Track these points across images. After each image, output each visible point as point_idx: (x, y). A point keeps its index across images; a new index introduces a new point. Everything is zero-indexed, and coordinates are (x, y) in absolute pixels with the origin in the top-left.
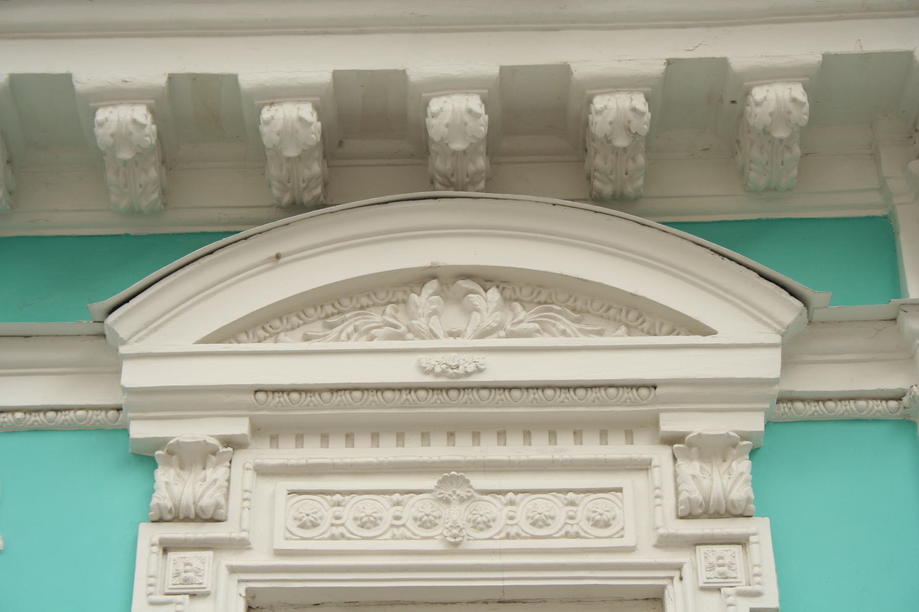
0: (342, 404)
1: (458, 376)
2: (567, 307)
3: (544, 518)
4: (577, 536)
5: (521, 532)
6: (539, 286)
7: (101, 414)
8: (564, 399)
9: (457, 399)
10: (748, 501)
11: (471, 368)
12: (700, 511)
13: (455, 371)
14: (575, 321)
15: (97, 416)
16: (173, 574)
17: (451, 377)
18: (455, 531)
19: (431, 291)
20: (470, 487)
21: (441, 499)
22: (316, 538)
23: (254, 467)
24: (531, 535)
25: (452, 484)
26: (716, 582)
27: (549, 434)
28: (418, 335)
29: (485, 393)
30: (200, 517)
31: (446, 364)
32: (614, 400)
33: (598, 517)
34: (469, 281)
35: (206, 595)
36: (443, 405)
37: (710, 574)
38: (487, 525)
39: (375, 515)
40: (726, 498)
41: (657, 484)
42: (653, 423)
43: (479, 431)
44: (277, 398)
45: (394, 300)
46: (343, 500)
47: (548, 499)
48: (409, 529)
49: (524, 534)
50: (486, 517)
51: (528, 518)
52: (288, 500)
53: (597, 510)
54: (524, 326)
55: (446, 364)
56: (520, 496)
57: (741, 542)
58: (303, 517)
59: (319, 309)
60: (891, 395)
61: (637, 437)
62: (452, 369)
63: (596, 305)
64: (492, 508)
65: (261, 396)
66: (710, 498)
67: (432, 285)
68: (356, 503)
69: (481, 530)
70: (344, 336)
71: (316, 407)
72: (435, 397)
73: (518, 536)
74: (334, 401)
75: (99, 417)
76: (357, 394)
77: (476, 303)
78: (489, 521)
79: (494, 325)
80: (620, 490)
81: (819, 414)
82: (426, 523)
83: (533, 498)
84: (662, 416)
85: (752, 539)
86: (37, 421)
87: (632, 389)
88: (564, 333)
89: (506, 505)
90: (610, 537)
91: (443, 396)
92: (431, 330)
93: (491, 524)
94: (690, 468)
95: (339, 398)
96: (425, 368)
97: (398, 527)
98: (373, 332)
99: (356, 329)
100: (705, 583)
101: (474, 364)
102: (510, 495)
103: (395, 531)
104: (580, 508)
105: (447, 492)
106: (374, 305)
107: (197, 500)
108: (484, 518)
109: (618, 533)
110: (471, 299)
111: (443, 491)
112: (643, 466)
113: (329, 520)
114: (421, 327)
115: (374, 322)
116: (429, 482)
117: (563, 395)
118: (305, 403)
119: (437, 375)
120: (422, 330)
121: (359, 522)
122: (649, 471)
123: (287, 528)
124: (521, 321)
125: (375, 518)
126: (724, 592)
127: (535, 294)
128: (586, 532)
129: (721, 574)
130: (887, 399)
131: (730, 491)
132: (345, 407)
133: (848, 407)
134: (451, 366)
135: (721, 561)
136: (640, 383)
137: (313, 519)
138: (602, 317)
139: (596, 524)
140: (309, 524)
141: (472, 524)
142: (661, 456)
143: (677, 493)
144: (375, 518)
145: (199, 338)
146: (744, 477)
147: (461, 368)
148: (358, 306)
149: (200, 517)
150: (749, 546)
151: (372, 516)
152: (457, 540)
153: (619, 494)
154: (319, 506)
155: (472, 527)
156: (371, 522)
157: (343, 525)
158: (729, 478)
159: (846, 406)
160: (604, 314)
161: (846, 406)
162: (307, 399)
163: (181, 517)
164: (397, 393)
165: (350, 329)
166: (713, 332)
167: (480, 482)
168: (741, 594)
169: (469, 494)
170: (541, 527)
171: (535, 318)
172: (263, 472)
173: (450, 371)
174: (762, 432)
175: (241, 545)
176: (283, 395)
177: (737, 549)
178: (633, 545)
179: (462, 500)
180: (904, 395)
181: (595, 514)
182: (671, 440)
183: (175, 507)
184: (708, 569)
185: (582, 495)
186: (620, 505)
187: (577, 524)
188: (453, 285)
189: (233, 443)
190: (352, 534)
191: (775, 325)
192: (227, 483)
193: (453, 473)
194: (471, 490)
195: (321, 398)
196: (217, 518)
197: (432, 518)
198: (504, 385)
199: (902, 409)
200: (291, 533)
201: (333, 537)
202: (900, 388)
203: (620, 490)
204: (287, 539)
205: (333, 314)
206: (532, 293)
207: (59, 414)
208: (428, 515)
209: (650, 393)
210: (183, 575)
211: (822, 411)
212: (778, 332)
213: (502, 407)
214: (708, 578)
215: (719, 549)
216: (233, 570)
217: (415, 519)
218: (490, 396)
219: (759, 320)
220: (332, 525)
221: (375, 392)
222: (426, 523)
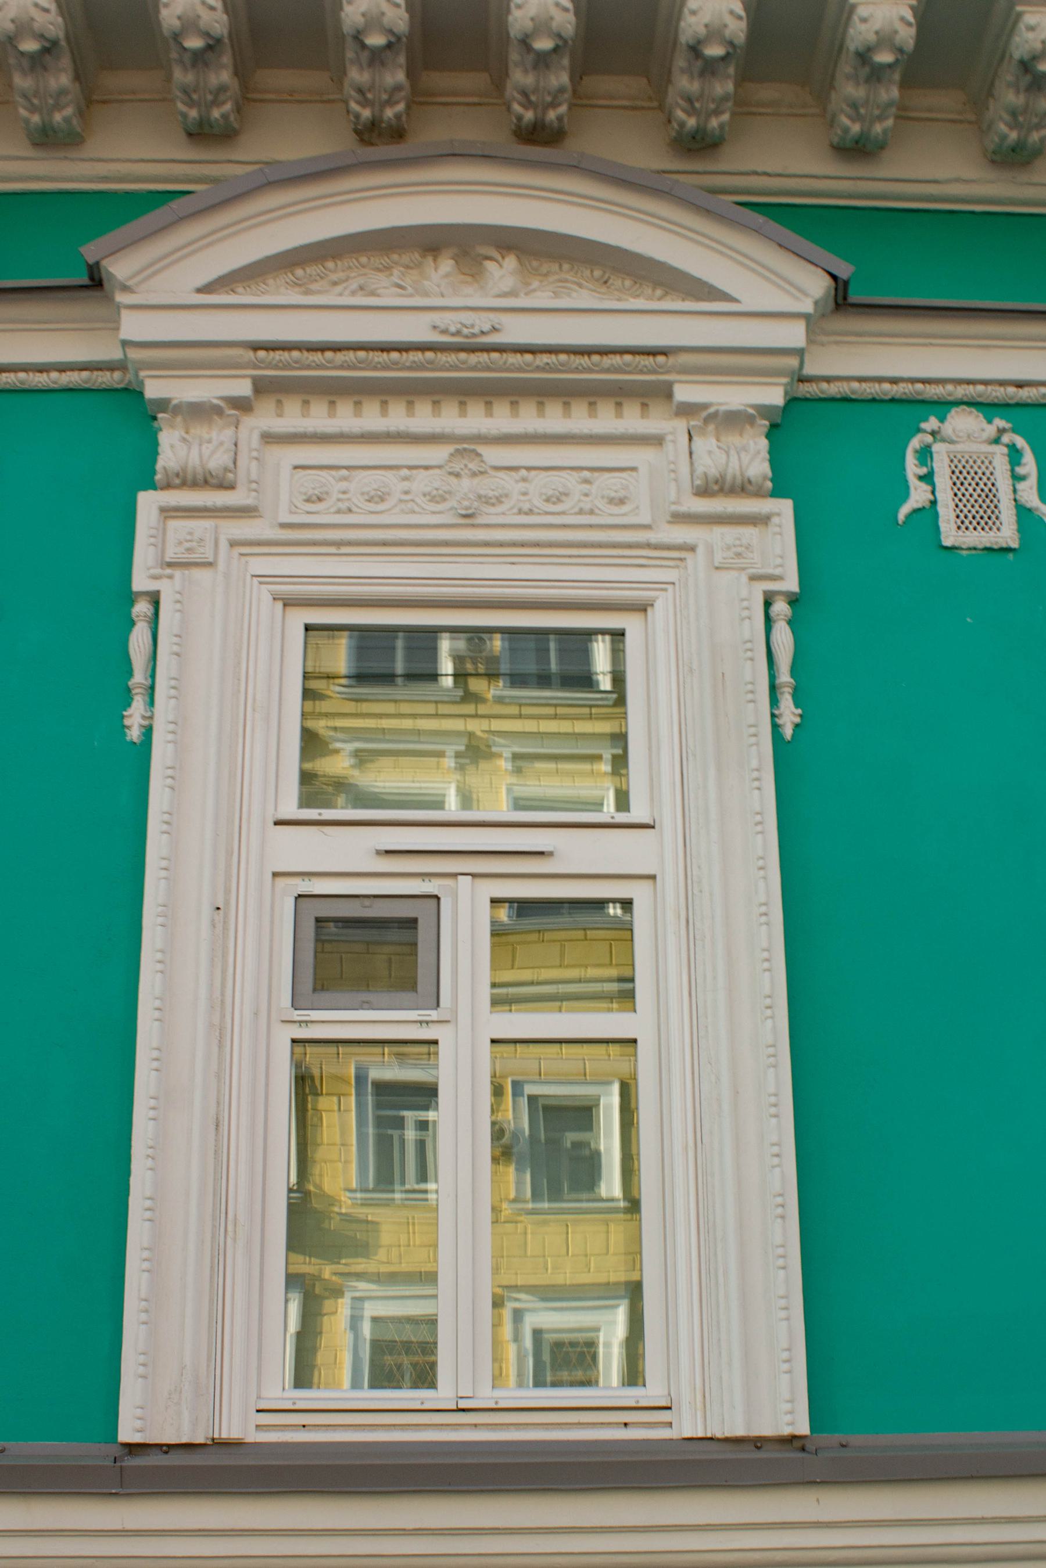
1: (474, 335)
3: (558, 494)
11: (486, 328)
17: (467, 337)
21: (450, 473)
25: (463, 457)
33: (613, 494)
38: (499, 500)
39: (382, 490)
40: (742, 475)
41: (671, 458)
42: (665, 392)
48: (417, 504)
51: (541, 494)
52: (292, 476)
56: (533, 473)
62: (467, 328)
64: (507, 482)
73: (530, 512)
82: (437, 498)
93: (503, 499)
94: (704, 444)
100: (720, 563)
103: (403, 506)
105: (457, 467)
108: (496, 494)
111: (454, 465)
112: (656, 441)
113: (335, 496)
119: (453, 335)
128: (599, 509)
139: (611, 501)
140: (314, 498)
153: (634, 474)
167: (494, 455)
169: (482, 469)
170: (554, 503)
172: (270, 438)
174: (776, 407)
179: (474, 474)
189: (242, 405)
192: (234, 447)
194: (484, 465)
201: (339, 512)
204: (291, 512)
208: (437, 489)
210: (734, 550)
220: (339, 500)
222: (437, 498)
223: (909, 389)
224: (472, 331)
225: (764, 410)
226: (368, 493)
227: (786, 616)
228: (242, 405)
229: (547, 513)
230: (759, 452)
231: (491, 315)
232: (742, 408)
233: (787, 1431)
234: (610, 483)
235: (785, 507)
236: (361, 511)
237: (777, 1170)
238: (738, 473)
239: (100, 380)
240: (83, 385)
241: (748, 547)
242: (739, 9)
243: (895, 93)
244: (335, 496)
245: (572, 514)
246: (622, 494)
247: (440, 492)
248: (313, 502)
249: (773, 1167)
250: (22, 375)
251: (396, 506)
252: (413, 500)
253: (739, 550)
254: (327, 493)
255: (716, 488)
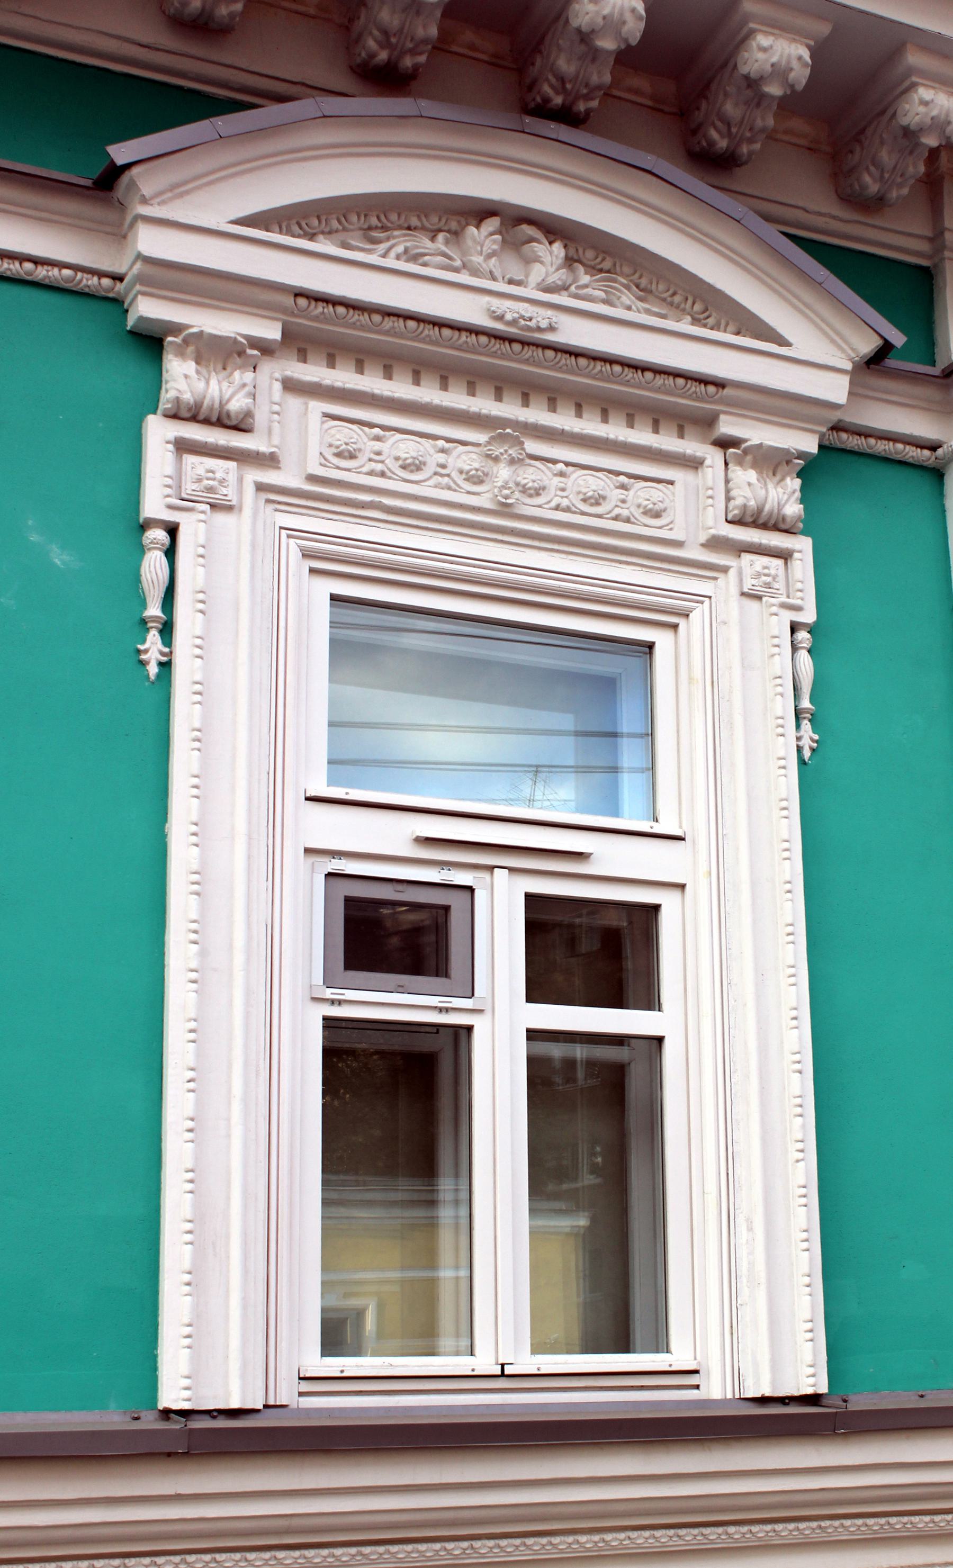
0: (358, 323)
1: (529, 329)
2: (631, 281)
3: (597, 496)
4: (628, 520)
5: (386, 470)
6: (604, 252)
7: (92, 279)
8: (497, 350)
9: (520, 353)
10: (799, 519)
11: (544, 324)
12: (187, 415)
13: (528, 323)
14: (641, 299)
15: (87, 280)
16: (192, 479)
18: (506, 492)
19: (491, 229)
20: (523, 449)
22: (354, 470)
23: (282, 379)
24: (581, 510)
26: (760, 590)
27: (468, 383)
28: (475, 273)
29: (550, 354)
30: (221, 421)
31: (518, 313)
32: (552, 363)
34: (533, 227)
35: (229, 508)
36: (503, 357)
37: (754, 582)
38: (537, 492)
39: (420, 458)
41: (710, 484)
42: (707, 422)
43: (447, 375)
44: (320, 308)
45: (446, 228)
46: (384, 436)
47: (599, 478)
49: (574, 509)
50: (538, 484)
53: (651, 499)
54: (589, 291)
55: (518, 313)
57: (785, 556)
58: (341, 445)
59: (363, 218)
60: (928, 444)
61: (688, 430)
62: (524, 320)
63: (661, 287)
65: (302, 302)
66: (202, 403)
67: (492, 224)
68: (396, 442)
69: (531, 496)
70: (393, 254)
71: (363, 328)
72: (496, 346)
73: (567, 510)
74: (385, 326)
75: (90, 282)
76: (411, 324)
77: (540, 254)
78: (540, 489)
79: (559, 283)
80: (671, 483)
81: (859, 448)
82: (477, 479)
83: (337, 425)
84: (722, 417)
85: (796, 555)
86: (9, 269)
87: (700, 383)
88: (629, 308)
89: (555, 475)
90: (660, 528)
91: (505, 347)
92: (491, 272)
93: (541, 491)
95: (530, 353)
96: (494, 312)
97: (442, 475)
98: (427, 258)
99: (406, 251)
100: (749, 589)
101: (547, 320)
102: (561, 466)
104: (631, 493)
105: (498, 450)
106: (423, 228)
107: (224, 402)
108: (536, 485)
109: (667, 525)
110: (536, 249)
114: (482, 267)
115: (427, 248)
116: (481, 437)
117: (629, 374)
118: (350, 321)
119: (509, 323)
120: (481, 269)
121: (400, 462)
122: (700, 470)
123: (321, 453)
124: (586, 286)
125: (420, 462)
126: (766, 602)
127: (599, 259)
128: (636, 519)
129: (765, 584)
130: (922, 447)
131: (228, 401)
132: (396, 335)
133: (887, 447)
134: (524, 316)
135: (766, 571)
136: (710, 379)
137: (351, 449)
138: (664, 300)
139: (647, 512)
140: (346, 454)
141: (520, 488)
142: (714, 457)
143: (728, 499)
144: (420, 462)
145: (232, 218)
146: (247, 389)
147: (534, 321)
148: (406, 225)
149: (221, 421)
150: (791, 562)
151: (418, 459)
152: (509, 501)
153: (670, 486)
154: (602, 483)
155: (465, 479)
156: (416, 465)
157: (382, 462)
158: (784, 493)
159: (885, 445)
160: (669, 299)
161: (885, 445)
162: (354, 316)
163: (201, 417)
164: (457, 333)
165: (400, 249)
166: (788, 344)
167: (533, 446)
168: (784, 606)
170: (592, 505)
171: (599, 285)
172: (291, 386)
173: (523, 322)
174: (275, 340)
175: (270, 461)
176: (328, 305)
177: (779, 562)
178: (683, 540)
180: (940, 447)
181: (648, 502)
182: (725, 443)
183: (196, 406)
184: (753, 577)
185: (632, 480)
186: (672, 498)
187: (628, 508)
188: (513, 227)
189: (266, 349)
190: (636, 519)
191: (850, 352)
193: (508, 431)
195: (370, 318)
196: (243, 426)
197: (481, 474)
198: (572, 350)
199: (933, 458)
200: (325, 459)
202: (938, 439)
203: (671, 483)
205: (376, 228)
206: (596, 258)
207: (40, 268)
209: (418, 327)
210: (206, 482)
211: (862, 445)
212: (851, 359)
213: (563, 372)
214: (753, 585)
215: (765, 560)
216: (261, 488)
217: (461, 472)
218: (555, 358)
219: (833, 341)
221: (431, 326)
223: (917, 454)
224: (528, 323)
225: (801, 455)
226: (338, 447)
227: (163, 545)
228: (266, 349)
229: (583, 513)
230: (794, 492)
231: (549, 313)
232: (233, 335)
233: (810, 1391)
234: (642, 494)
235: (803, 545)
236: (329, 464)
237: (802, 1164)
238: (217, 405)
239: (911, 454)
240: (868, 450)
241: (222, 481)
242: (641, 8)
243: (770, 122)
244: (553, 491)
245: (355, 472)
246: (660, 506)
247: (480, 473)
248: (345, 458)
249: (798, 1161)
250: (900, 446)
251: (431, 477)
252: (448, 475)
253: (768, 579)
254: (360, 450)
255: (750, 520)
